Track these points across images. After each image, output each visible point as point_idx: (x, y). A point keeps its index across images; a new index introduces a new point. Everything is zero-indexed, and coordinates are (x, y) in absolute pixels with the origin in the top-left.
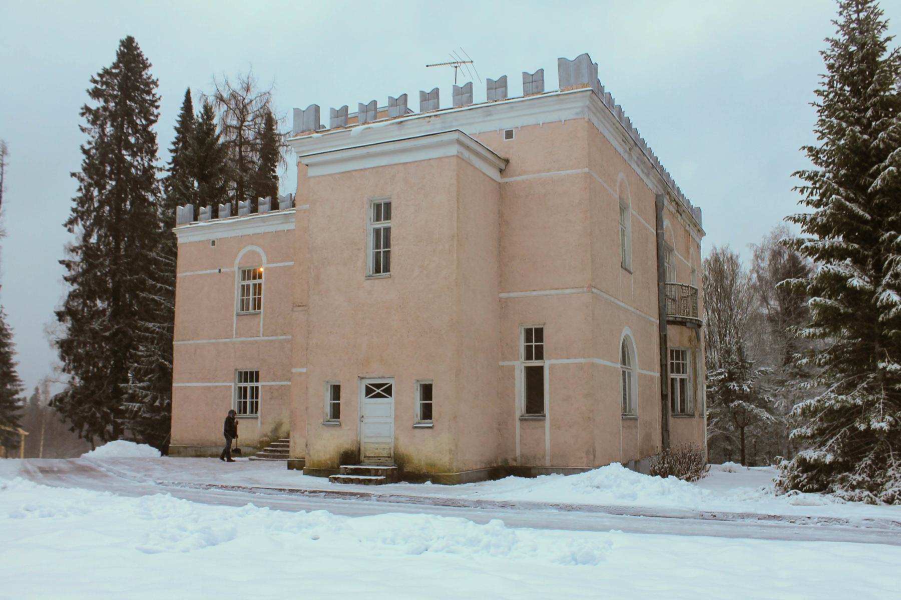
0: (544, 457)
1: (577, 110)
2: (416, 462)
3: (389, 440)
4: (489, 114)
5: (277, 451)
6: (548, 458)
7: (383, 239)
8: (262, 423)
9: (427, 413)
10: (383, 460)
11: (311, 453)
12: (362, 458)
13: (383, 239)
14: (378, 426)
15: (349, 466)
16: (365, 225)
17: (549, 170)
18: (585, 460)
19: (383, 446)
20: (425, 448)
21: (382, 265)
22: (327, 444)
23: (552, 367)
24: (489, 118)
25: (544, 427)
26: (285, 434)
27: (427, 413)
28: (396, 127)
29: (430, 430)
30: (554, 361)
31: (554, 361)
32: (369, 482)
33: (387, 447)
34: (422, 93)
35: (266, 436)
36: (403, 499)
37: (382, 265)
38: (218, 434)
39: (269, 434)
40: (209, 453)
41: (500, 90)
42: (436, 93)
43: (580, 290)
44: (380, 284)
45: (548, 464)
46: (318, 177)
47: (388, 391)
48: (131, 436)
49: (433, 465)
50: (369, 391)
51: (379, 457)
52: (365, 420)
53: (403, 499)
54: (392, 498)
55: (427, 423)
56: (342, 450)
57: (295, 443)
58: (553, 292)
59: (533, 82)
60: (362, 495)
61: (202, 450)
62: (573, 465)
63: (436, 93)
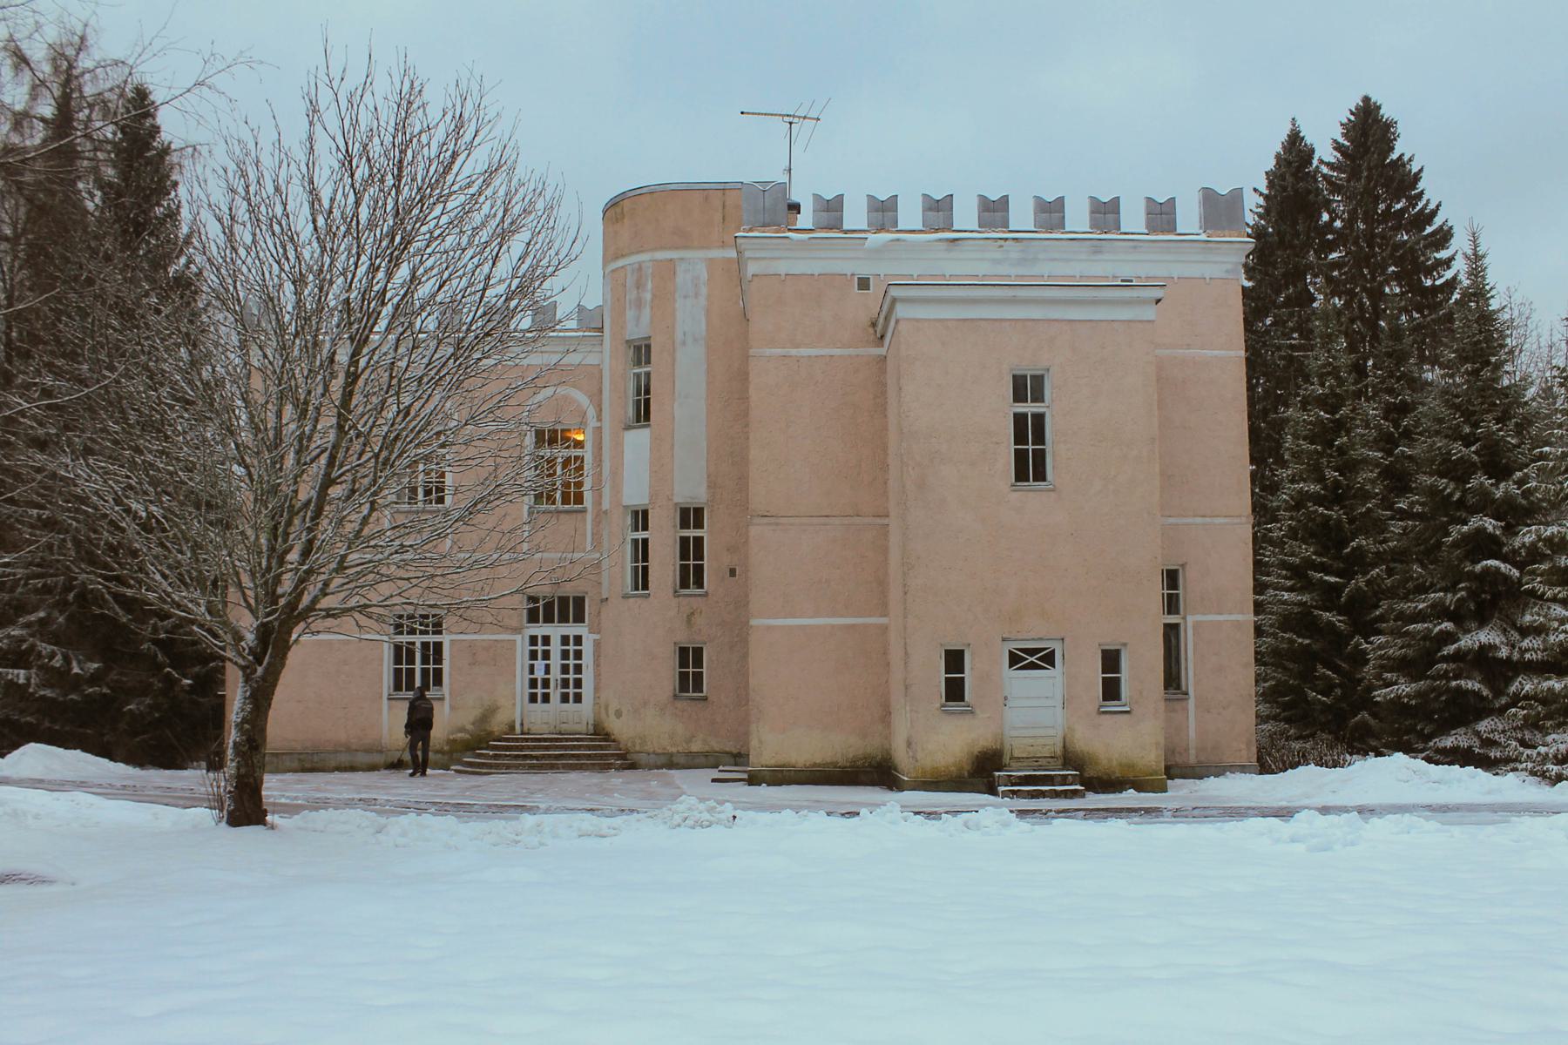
0: (1187, 750)
1: (1229, 267)
2: (1105, 762)
3: (1051, 732)
4: (1097, 251)
5: (532, 757)
6: (1192, 752)
7: (1029, 430)
8: (452, 708)
9: (1111, 690)
10: (1043, 762)
11: (919, 756)
12: (1006, 759)
13: (1029, 430)
14: (1034, 711)
15: (983, 773)
16: (1001, 412)
17: (1189, 346)
18: (1244, 753)
19: (1041, 741)
20: (1128, 739)
21: (1030, 467)
22: (950, 740)
23: (1197, 625)
24: (1099, 257)
25: (1186, 710)
26: (505, 728)
27: (1111, 690)
28: (944, 245)
29: (1126, 716)
30: (1199, 618)
31: (1199, 618)
32: (1042, 794)
33: (1050, 742)
34: (983, 200)
35: (462, 730)
36: (1215, 812)
37: (1030, 467)
38: (391, 723)
39: (470, 727)
40: (333, 764)
41: (1110, 217)
42: (1004, 202)
43: (1237, 520)
44: (1032, 496)
45: (1192, 760)
46: (917, 320)
47: (1049, 659)
48: (296, 764)
49: (1131, 766)
50: (1014, 659)
51: (1037, 759)
52: (1010, 704)
53: (1215, 812)
54: (1196, 812)
55: (1112, 706)
56: (976, 750)
57: (761, 742)
58: (1199, 520)
59: (1161, 215)
60: (1148, 811)
61: (316, 758)
62: (1229, 760)
63: (1004, 202)
